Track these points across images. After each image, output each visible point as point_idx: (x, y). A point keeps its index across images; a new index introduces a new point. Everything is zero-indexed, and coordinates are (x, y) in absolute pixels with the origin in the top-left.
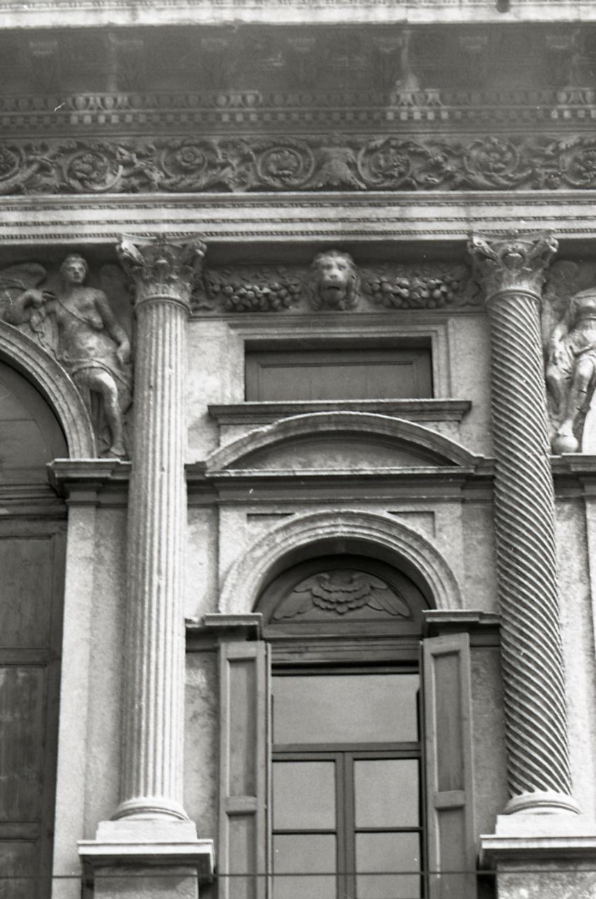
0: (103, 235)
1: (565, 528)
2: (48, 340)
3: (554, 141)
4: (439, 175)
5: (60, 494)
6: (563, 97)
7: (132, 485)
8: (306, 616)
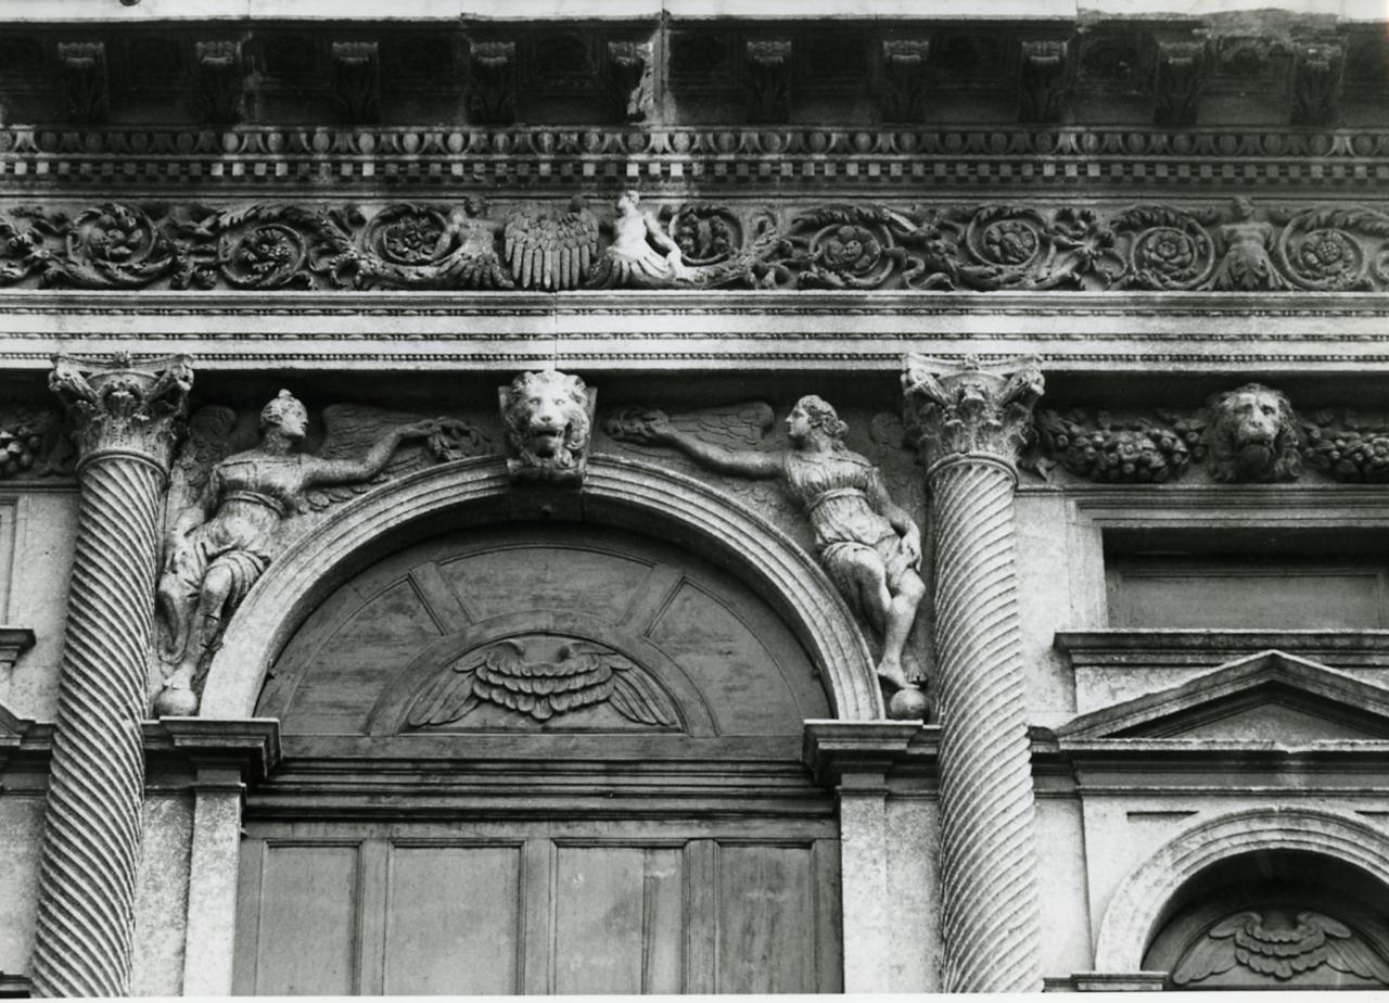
1: (158, 839)
3: (214, 212)
4: (26, 264)
5: (817, 779)
6: (231, 141)
7: (949, 762)
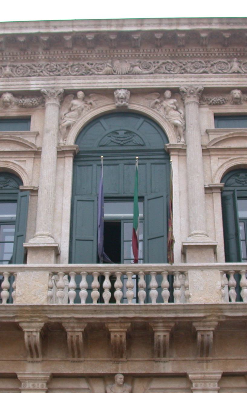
0: (232, 85)
2: (162, 112)
8: (234, 185)
